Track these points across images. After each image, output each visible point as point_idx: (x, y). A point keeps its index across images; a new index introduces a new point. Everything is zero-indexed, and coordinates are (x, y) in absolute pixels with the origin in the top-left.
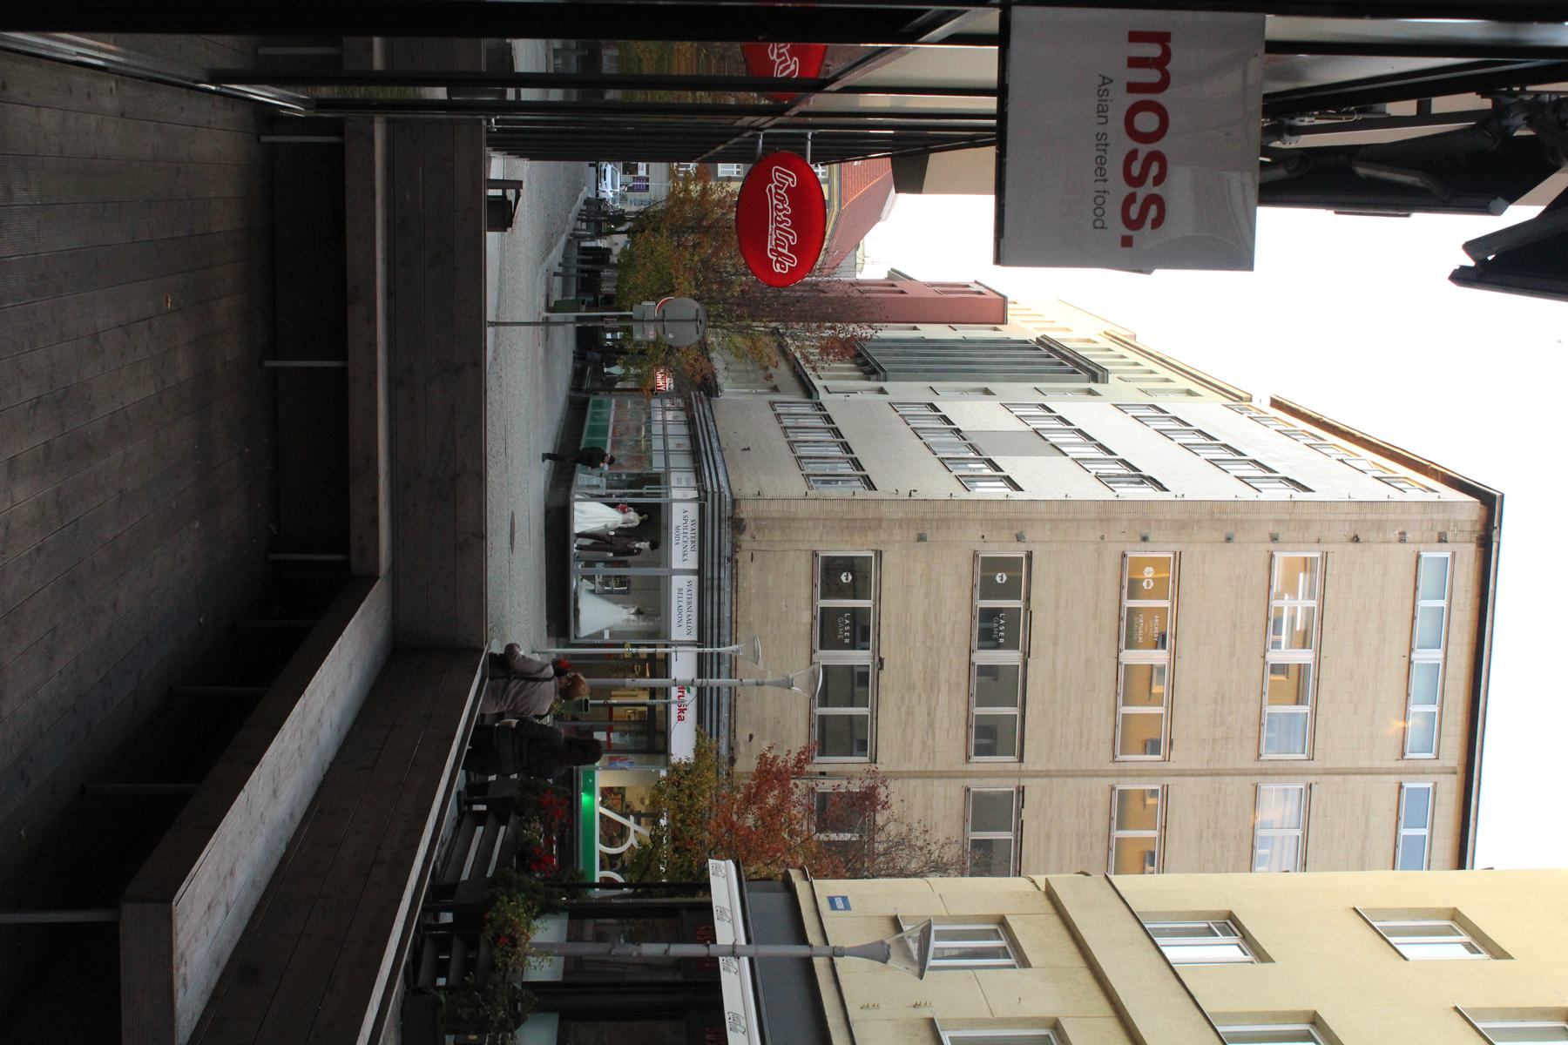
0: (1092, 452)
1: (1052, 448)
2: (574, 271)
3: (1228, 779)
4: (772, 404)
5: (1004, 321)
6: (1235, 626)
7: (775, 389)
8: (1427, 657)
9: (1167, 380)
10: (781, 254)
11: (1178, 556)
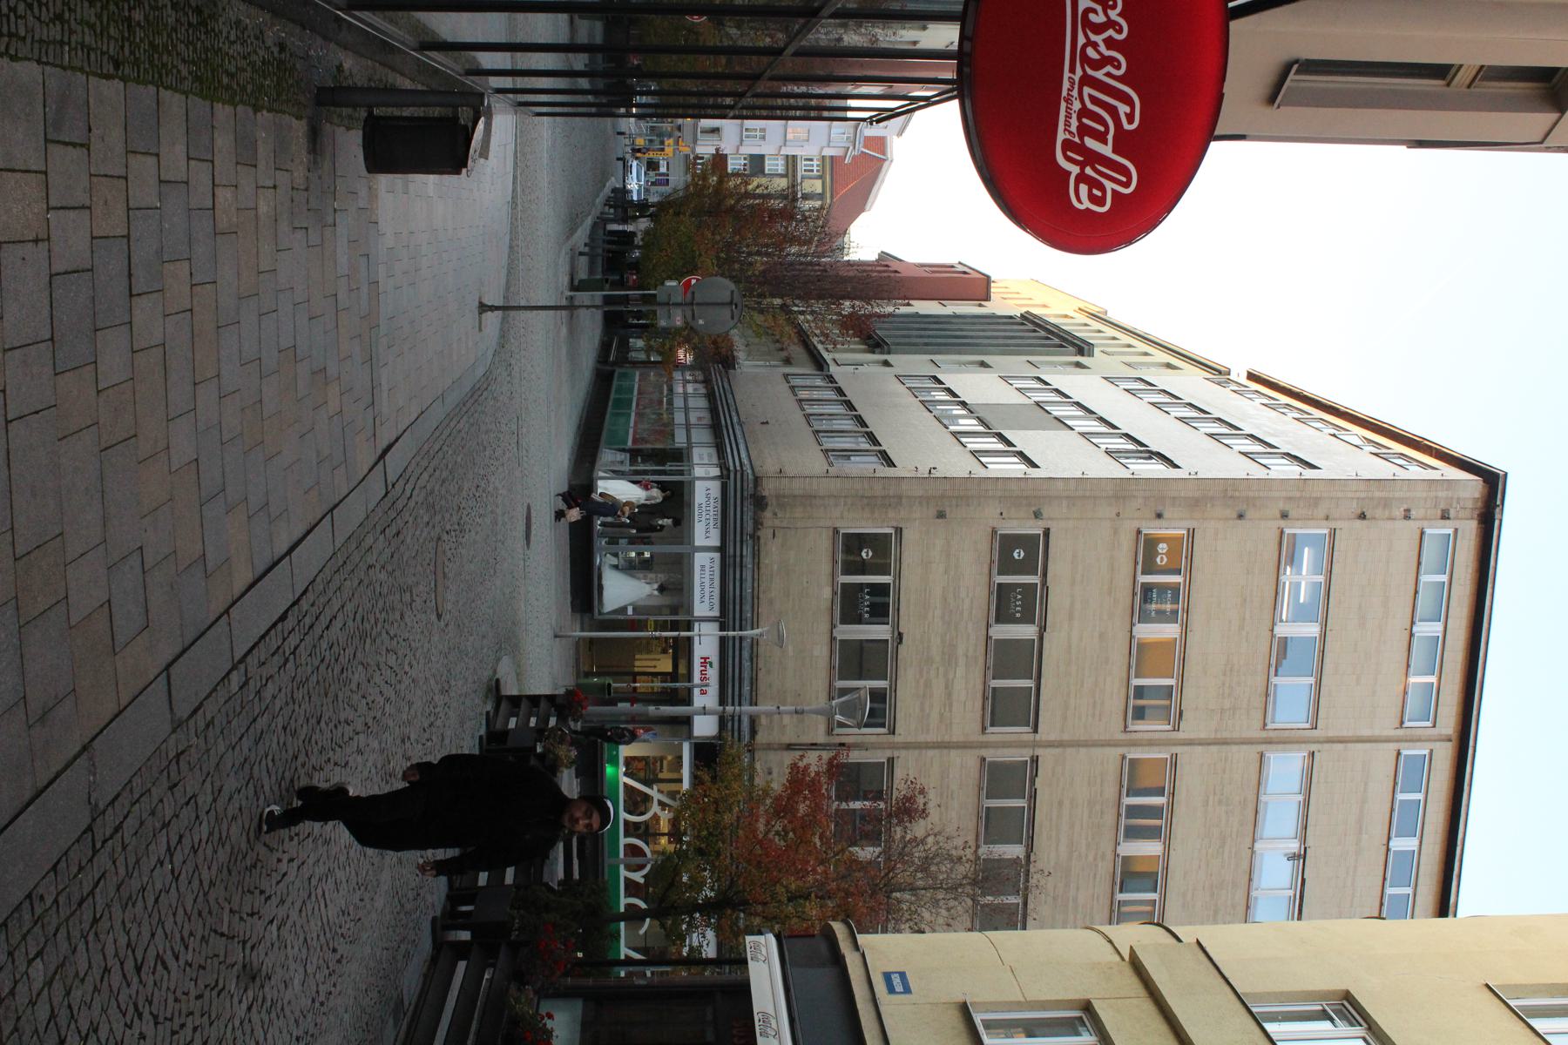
0: (1093, 426)
1: (1056, 421)
2: (600, 251)
3: (1235, 748)
4: (786, 376)
5: (988, 298)
6: (1245, 600)
7: (788, 361)
8: (1427, 629)
9: (1146, 354)
10: (1093, 158)
11: (1192, 533)
